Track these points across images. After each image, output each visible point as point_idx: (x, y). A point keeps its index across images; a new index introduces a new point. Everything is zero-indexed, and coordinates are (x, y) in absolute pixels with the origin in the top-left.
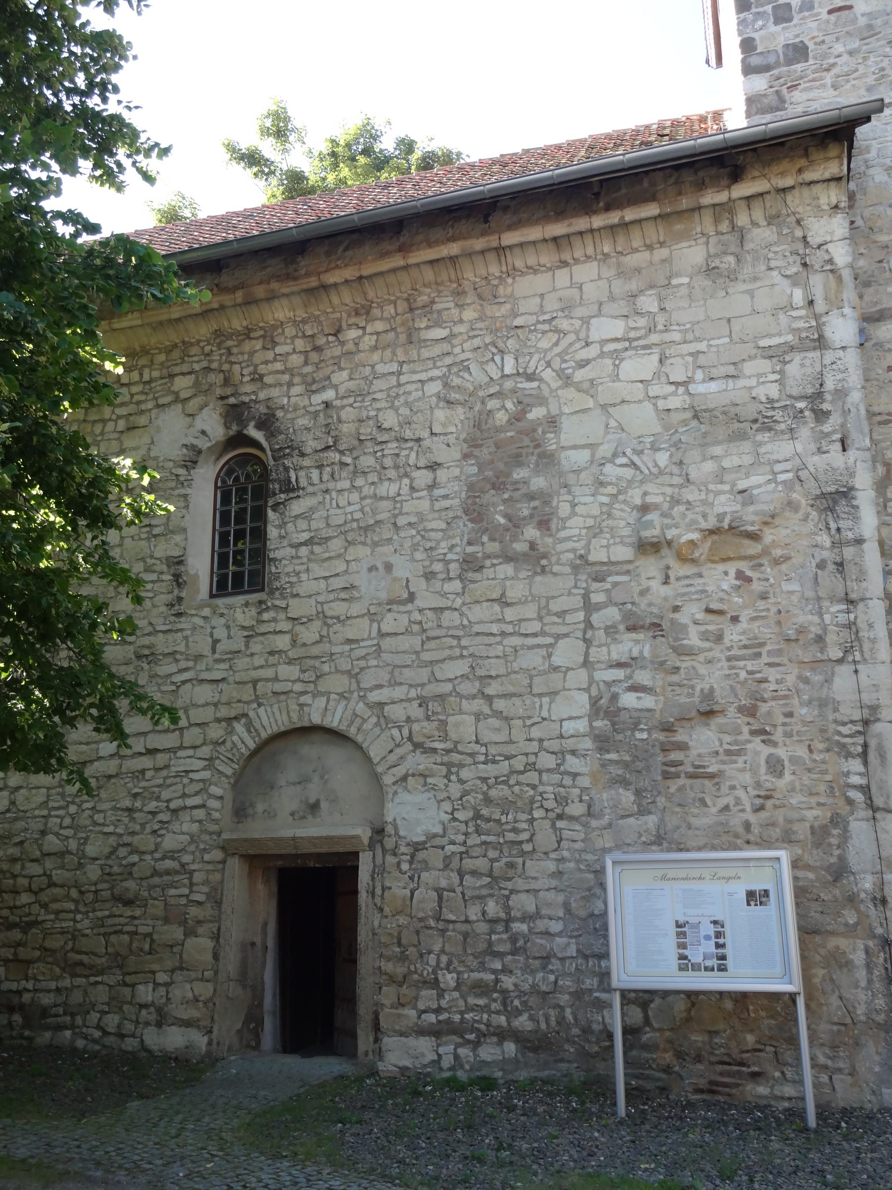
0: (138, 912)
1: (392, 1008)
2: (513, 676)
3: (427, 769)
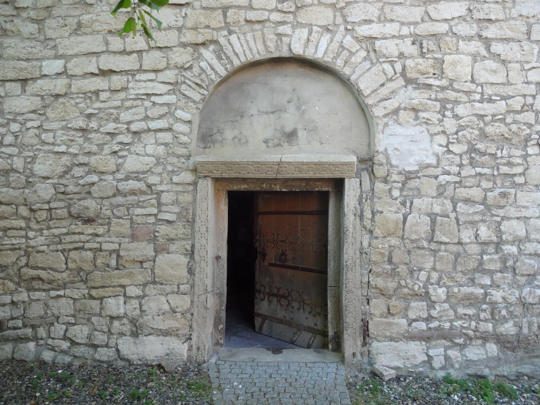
0: (100, 230)
1: (381, 317)
2: (512, 22)
3: (421, 104)
